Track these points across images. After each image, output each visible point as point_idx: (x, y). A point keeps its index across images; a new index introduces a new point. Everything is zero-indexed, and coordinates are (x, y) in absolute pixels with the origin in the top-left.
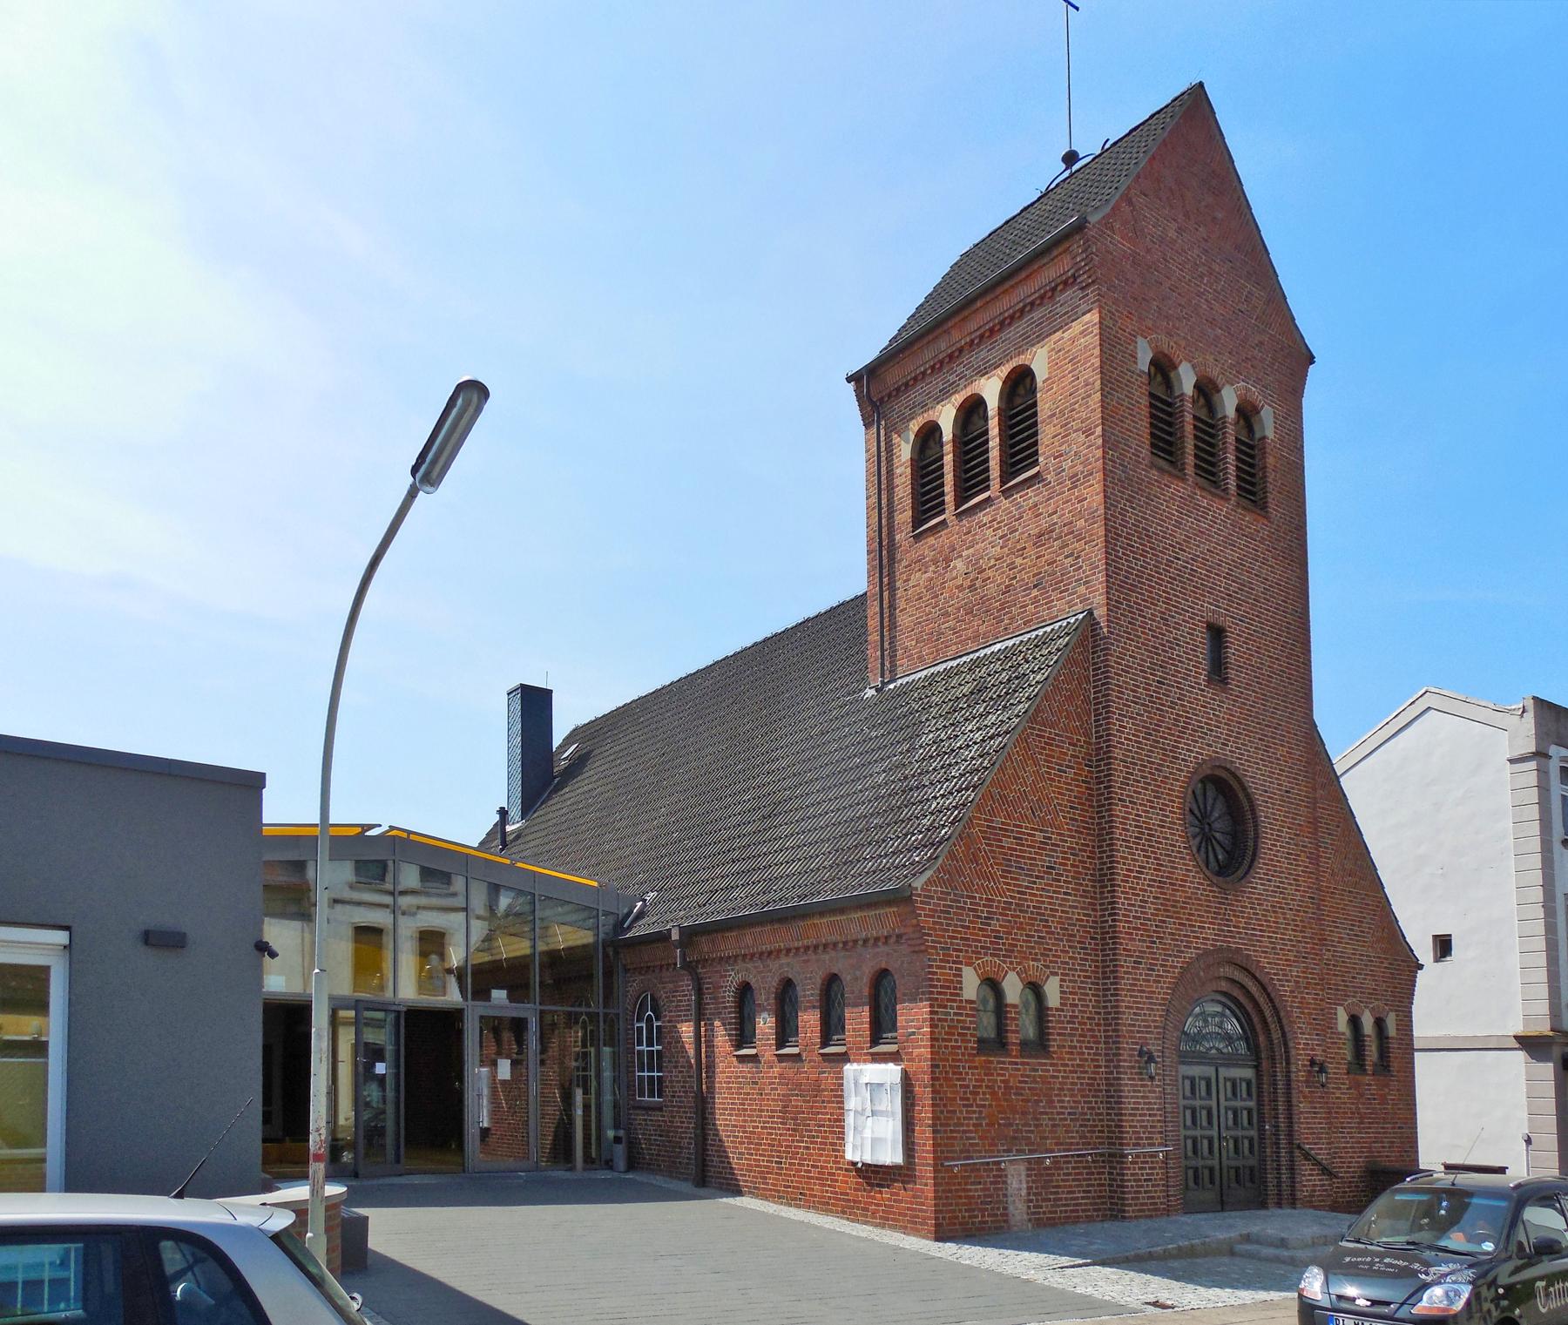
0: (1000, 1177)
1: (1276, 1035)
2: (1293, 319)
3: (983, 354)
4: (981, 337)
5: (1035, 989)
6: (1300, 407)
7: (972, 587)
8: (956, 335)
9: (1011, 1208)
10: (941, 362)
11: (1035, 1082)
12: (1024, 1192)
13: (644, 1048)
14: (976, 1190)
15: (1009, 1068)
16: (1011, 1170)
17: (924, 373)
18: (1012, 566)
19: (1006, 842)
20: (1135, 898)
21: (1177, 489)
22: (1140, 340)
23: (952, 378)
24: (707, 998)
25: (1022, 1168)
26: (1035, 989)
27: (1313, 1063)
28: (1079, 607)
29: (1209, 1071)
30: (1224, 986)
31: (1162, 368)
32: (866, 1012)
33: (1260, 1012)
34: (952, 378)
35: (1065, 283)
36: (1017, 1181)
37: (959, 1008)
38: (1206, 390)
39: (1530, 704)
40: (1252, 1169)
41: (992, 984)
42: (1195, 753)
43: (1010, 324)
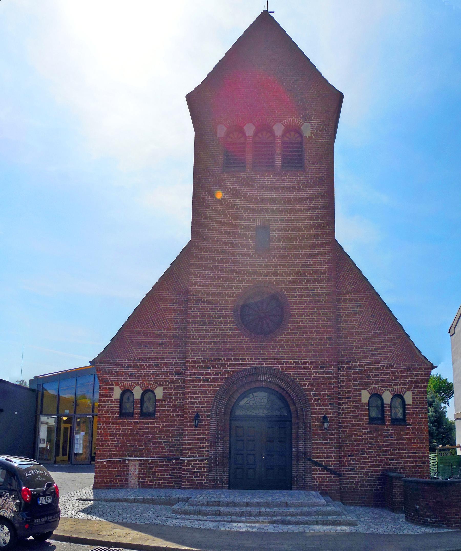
0: (126, 466)
2: (342, 249)
9: (130, 479)
11: (146, 429)
12: (137, 473)
14: (114, 471)
15: (131, 424)
16: (131, 464)
25: (137, 463)
32: (407, 403)
36: (134, 469)
37: (111, 402)
41: (376, 396)
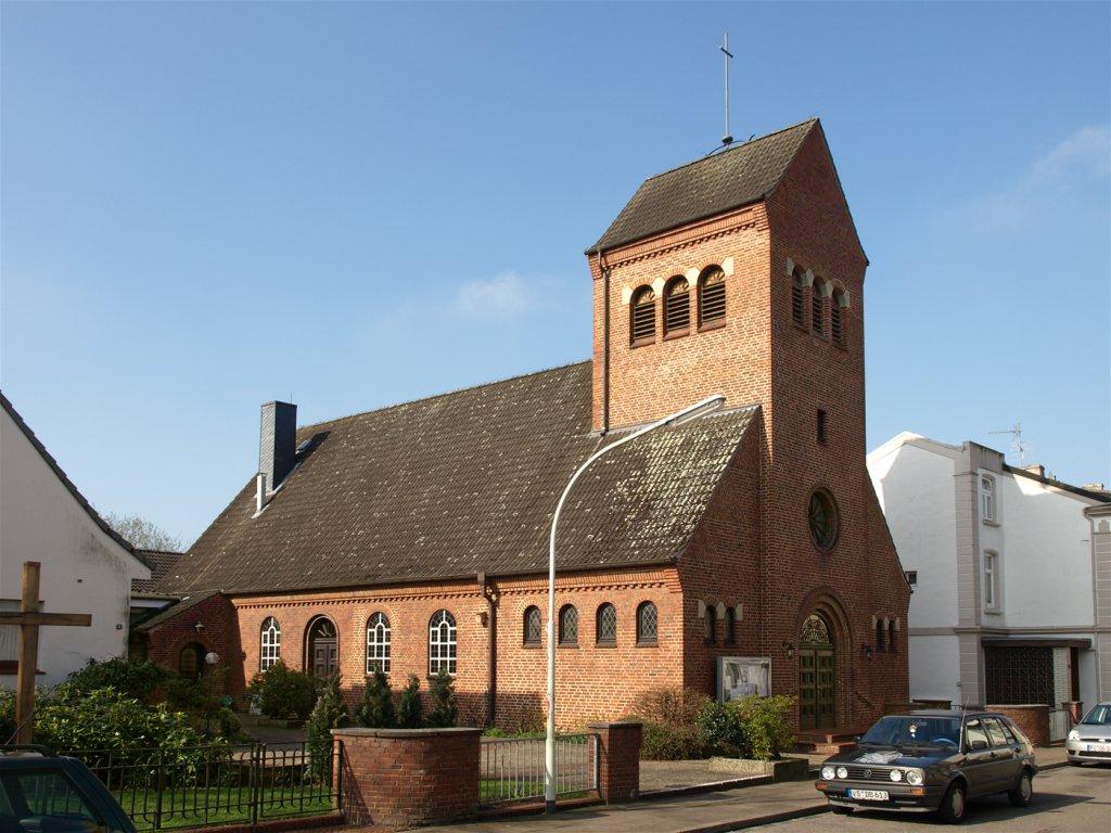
3: (687, 253)
5: (731, 611)
6: (862, 290)
8: (668, 240)
10: (656, 253)
18: (705, 374)
19: (720, 532)
22: (789, 260)
23: (663, 263)
26: (731, 611)
27: (863, 646)
28: (753, 401)
29: (812, 653)
30: (820, 607)
33: (836, 615)
34: (663, 263)
35: (748, 226)
39: (968, 445)
40: (811, 706)
42: (810, 481)
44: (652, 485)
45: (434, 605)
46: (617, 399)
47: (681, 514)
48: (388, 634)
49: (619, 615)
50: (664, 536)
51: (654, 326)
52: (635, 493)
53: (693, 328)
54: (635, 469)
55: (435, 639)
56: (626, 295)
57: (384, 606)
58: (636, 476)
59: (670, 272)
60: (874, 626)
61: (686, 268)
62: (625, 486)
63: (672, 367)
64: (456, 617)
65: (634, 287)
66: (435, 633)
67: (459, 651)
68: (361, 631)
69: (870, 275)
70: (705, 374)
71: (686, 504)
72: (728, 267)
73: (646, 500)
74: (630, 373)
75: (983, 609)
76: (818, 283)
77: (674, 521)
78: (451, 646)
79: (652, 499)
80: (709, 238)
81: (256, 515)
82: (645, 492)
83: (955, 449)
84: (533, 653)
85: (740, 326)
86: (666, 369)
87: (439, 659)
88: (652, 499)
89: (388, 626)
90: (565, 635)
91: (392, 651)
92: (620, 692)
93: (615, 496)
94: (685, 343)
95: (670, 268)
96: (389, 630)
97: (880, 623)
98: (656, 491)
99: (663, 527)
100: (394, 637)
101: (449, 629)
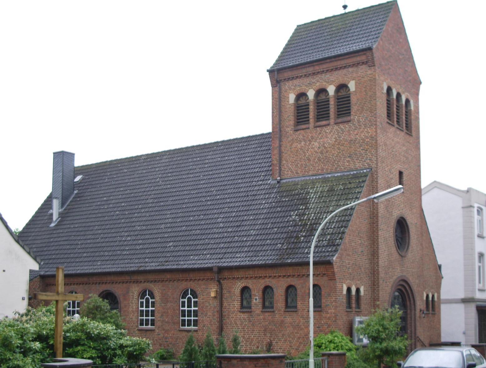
1: (412, 302)
3: (327, 76)
4: (327, 70)
7: (322, 153)
13: (144, 309)
17: (301, 76)
20: (383, 260)
21: (392, 129)
23: (313, 81)
24: (225, 291)
26: (358, 290)
31: (389, 90)
34: (313, 81)
38: (399, 95)
43: (339, 70)
44: (313, 215)
45: (183, 285)
46: (287, 161)
47: (332, 234)
48: (153, 303)
49: (299, 292)
50: (323, 246)
51: (308, 117)
52: (303, 220)
53: (332, 121)
54: (301, 204)
55: (142, 306)
56: (292, 98)
57: (151, 286)
58: (302, 209)
59: (318, 86)
60: (425, 298)
61: (327, 84)
62: (296, 215)
63: (319, 143)
64: (198, 293)
65: (297, 93)
66: (142, 303)
67: (199, 314)
68: (135, 301)
69: (422, 87)
70: (339, 149)
71: (334, 227)
72: (352, 86)
73: (311, 224)
74: (294, 145)
75: (477, 287)
76: (399, 95)
77: (329, 237)
78: (194, 310)
79: (314, 224)
80: (341, 68)
81: (53, 225)
82: (309, 219)
83: (463, 191)
84: (246, 316)
85: (359, 121)
86: (316, 144)
87: (144, 318)
88: (314, 224)
89: (153, 297)
90: (267, 304)
91: (156, 314)
92: (299, 338)
93: (291, 221)
94: (327, 130)
95: (318, 84)
96: (153, 300)
97: (349, 290)
98: (316, 218)
99: (323, 241)
100: (157, 305)
101: (193, 300)
